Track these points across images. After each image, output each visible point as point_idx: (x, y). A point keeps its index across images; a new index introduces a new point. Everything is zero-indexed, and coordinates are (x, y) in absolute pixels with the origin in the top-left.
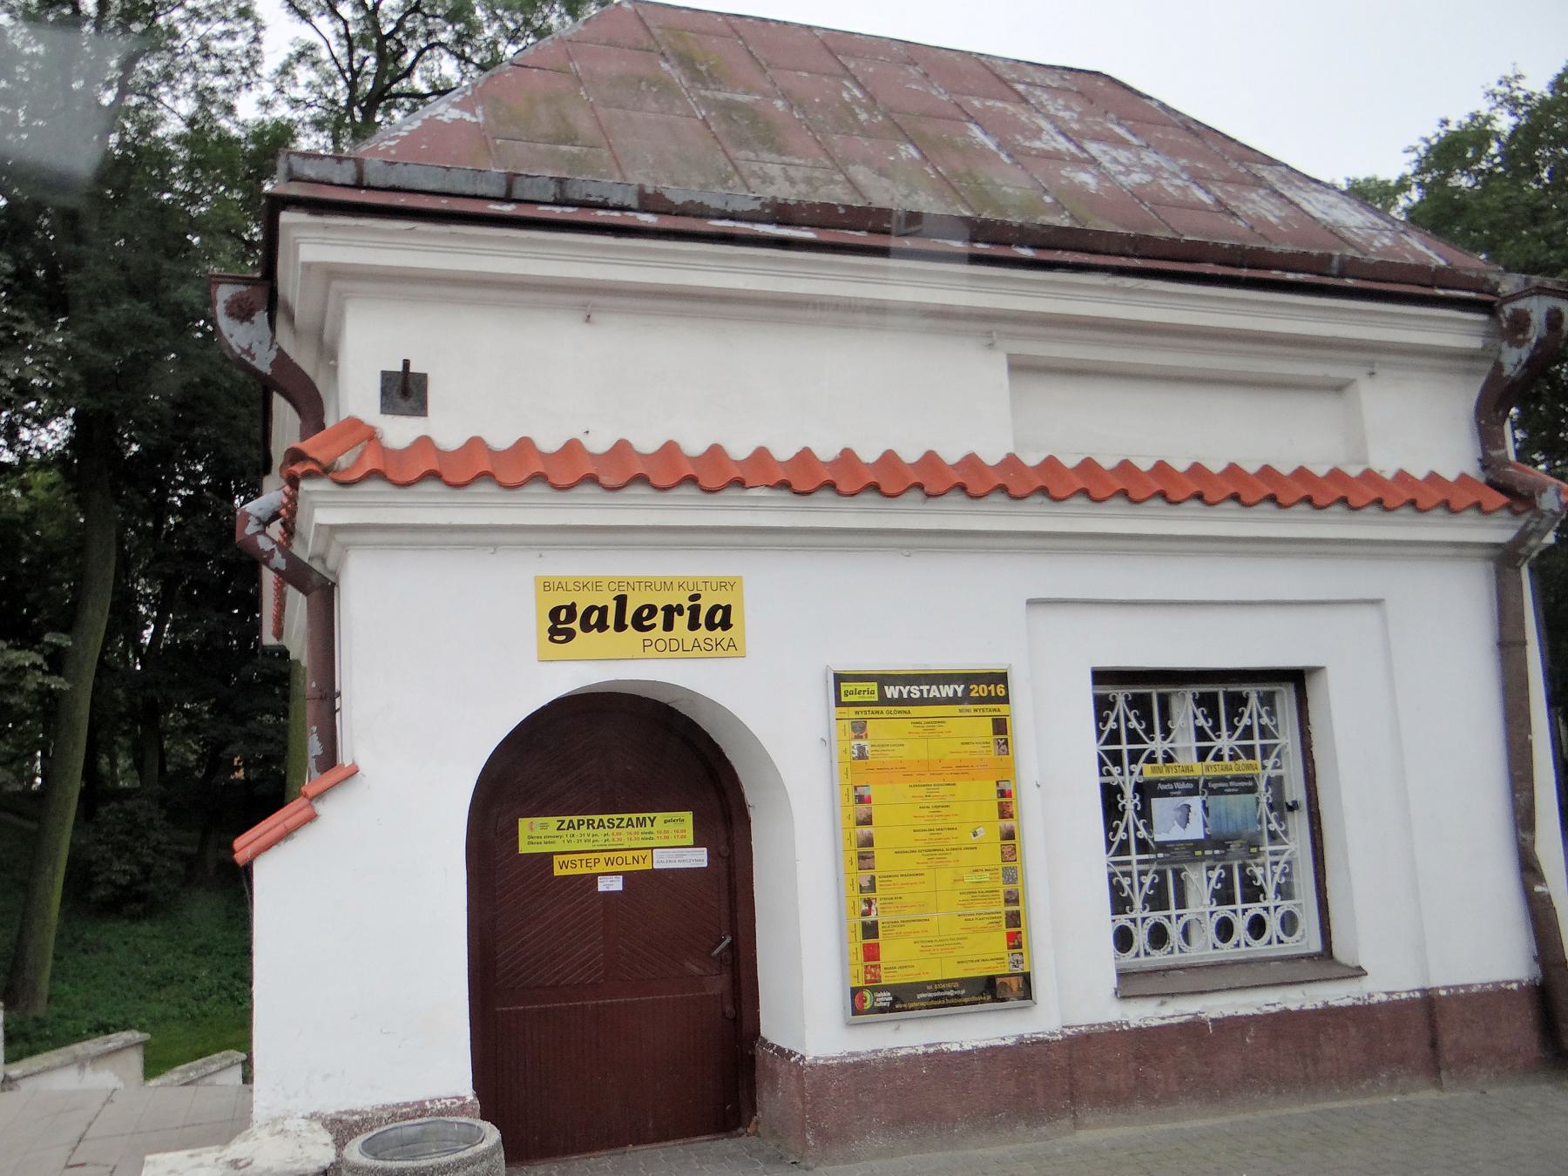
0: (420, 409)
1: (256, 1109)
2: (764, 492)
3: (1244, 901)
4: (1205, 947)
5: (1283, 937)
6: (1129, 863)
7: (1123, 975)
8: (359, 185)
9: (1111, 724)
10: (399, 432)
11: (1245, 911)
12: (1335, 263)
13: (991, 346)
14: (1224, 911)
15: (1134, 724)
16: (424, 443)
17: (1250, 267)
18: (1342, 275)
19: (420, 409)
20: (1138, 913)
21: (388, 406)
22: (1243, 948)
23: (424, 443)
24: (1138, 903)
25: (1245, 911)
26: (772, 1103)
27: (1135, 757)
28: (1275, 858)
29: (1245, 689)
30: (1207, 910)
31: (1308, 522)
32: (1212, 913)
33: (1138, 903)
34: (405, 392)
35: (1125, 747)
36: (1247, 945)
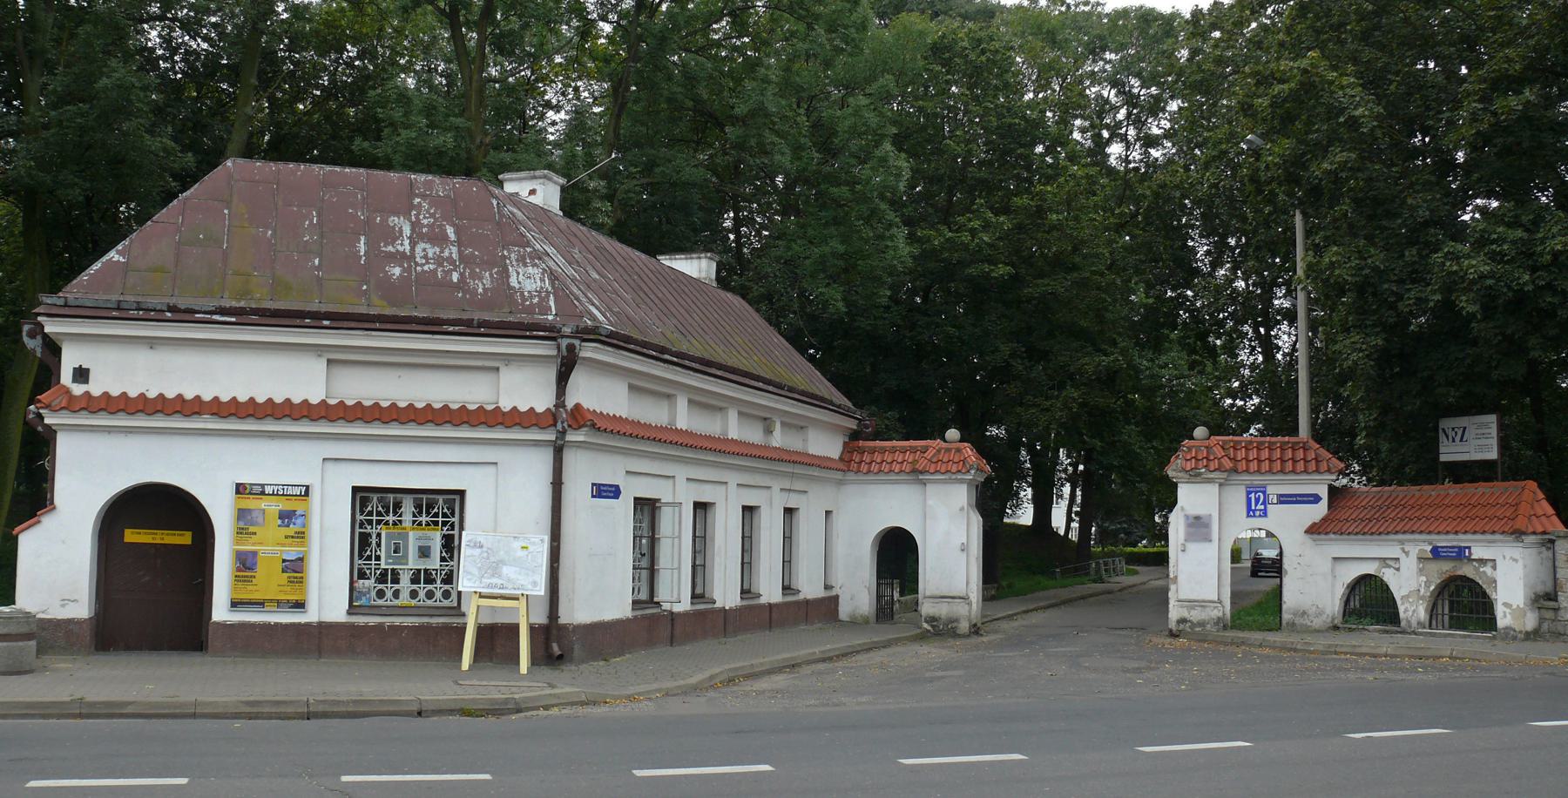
0: (86, 382)
1: (840, 609)
2: (208, 416)
3: (424, 584)
4: (404, 599)
5: (442, 600)
6: (371, 564)
7: (634, 602)
8: (66, 305)
9: (369, 508)
10: (78, 390)
11: (424, 588)
12: (475, 322)
13: (319, 356)
14: (415, 587)
15: (446, 510)
16: (87, 393)
17: (618, 340)
18: (479, 327)
19: (86, 382)
20: (438, 584)
21: (75, 380)
22: (389, 602)
23: (87, 393)
24: (439, 582)
25: (424, 588)
26: (213, 639)
27: (379, 522)
28: (378, 567)
29: (371, 495)
30: (373, 585)
31: (503, 432)
32: (375, 587)
33: (439, 582)
34: (81, 376)
35: (440, 519)
36: (440, 601)
